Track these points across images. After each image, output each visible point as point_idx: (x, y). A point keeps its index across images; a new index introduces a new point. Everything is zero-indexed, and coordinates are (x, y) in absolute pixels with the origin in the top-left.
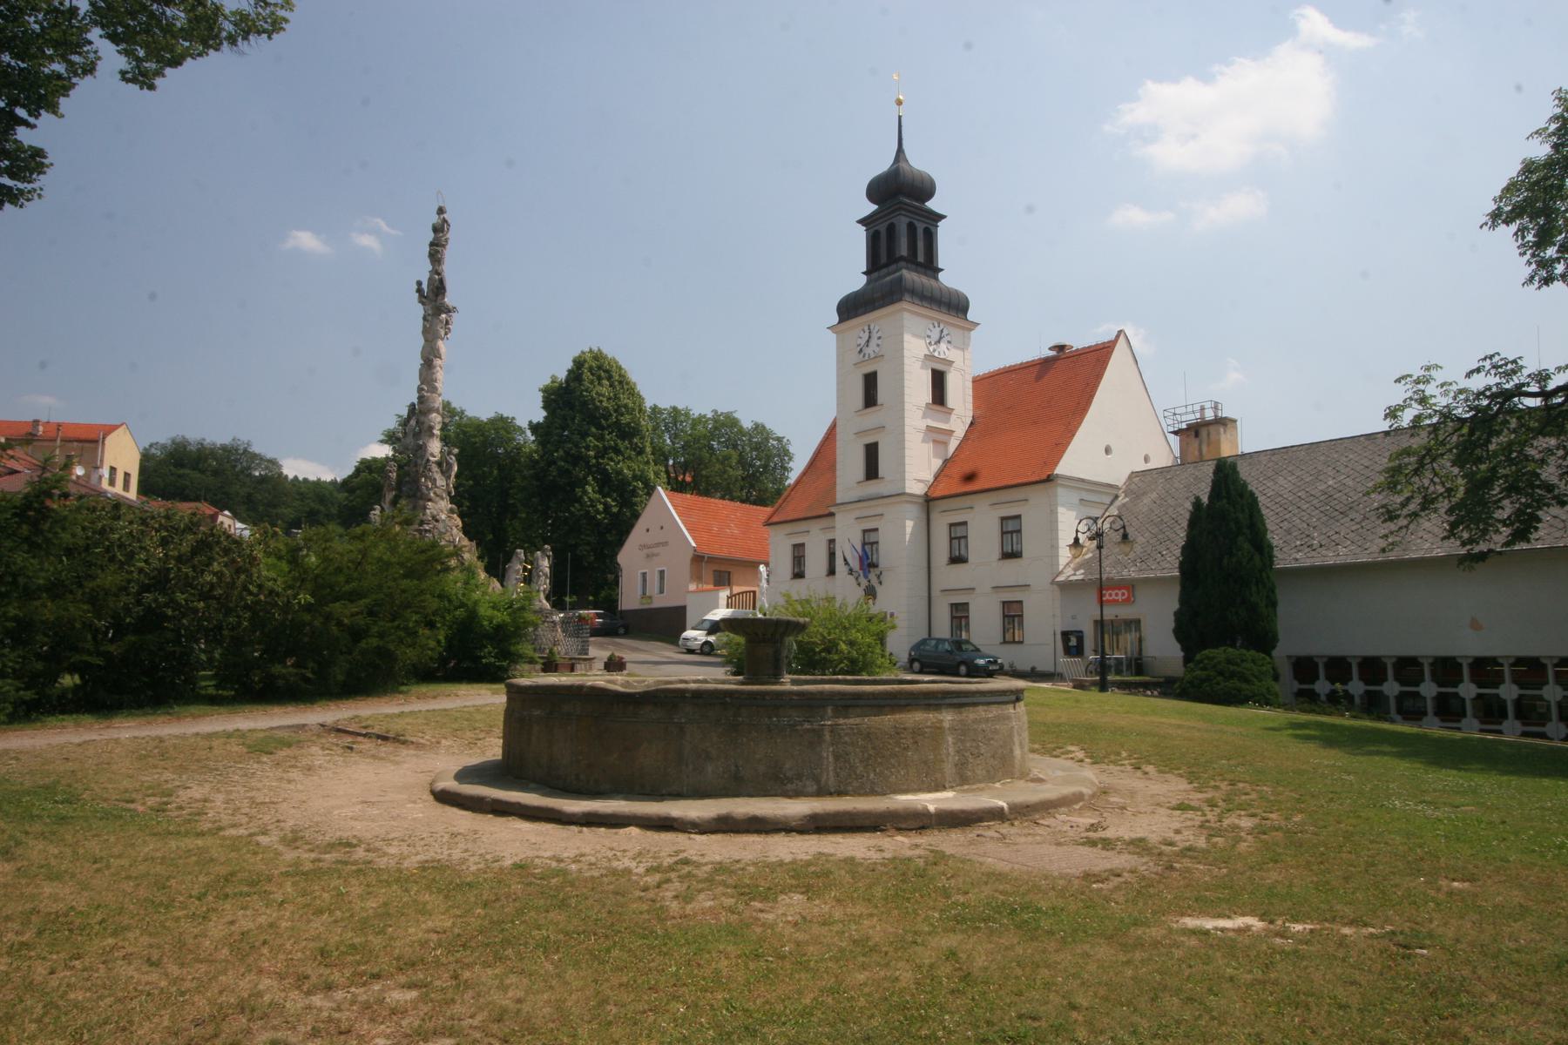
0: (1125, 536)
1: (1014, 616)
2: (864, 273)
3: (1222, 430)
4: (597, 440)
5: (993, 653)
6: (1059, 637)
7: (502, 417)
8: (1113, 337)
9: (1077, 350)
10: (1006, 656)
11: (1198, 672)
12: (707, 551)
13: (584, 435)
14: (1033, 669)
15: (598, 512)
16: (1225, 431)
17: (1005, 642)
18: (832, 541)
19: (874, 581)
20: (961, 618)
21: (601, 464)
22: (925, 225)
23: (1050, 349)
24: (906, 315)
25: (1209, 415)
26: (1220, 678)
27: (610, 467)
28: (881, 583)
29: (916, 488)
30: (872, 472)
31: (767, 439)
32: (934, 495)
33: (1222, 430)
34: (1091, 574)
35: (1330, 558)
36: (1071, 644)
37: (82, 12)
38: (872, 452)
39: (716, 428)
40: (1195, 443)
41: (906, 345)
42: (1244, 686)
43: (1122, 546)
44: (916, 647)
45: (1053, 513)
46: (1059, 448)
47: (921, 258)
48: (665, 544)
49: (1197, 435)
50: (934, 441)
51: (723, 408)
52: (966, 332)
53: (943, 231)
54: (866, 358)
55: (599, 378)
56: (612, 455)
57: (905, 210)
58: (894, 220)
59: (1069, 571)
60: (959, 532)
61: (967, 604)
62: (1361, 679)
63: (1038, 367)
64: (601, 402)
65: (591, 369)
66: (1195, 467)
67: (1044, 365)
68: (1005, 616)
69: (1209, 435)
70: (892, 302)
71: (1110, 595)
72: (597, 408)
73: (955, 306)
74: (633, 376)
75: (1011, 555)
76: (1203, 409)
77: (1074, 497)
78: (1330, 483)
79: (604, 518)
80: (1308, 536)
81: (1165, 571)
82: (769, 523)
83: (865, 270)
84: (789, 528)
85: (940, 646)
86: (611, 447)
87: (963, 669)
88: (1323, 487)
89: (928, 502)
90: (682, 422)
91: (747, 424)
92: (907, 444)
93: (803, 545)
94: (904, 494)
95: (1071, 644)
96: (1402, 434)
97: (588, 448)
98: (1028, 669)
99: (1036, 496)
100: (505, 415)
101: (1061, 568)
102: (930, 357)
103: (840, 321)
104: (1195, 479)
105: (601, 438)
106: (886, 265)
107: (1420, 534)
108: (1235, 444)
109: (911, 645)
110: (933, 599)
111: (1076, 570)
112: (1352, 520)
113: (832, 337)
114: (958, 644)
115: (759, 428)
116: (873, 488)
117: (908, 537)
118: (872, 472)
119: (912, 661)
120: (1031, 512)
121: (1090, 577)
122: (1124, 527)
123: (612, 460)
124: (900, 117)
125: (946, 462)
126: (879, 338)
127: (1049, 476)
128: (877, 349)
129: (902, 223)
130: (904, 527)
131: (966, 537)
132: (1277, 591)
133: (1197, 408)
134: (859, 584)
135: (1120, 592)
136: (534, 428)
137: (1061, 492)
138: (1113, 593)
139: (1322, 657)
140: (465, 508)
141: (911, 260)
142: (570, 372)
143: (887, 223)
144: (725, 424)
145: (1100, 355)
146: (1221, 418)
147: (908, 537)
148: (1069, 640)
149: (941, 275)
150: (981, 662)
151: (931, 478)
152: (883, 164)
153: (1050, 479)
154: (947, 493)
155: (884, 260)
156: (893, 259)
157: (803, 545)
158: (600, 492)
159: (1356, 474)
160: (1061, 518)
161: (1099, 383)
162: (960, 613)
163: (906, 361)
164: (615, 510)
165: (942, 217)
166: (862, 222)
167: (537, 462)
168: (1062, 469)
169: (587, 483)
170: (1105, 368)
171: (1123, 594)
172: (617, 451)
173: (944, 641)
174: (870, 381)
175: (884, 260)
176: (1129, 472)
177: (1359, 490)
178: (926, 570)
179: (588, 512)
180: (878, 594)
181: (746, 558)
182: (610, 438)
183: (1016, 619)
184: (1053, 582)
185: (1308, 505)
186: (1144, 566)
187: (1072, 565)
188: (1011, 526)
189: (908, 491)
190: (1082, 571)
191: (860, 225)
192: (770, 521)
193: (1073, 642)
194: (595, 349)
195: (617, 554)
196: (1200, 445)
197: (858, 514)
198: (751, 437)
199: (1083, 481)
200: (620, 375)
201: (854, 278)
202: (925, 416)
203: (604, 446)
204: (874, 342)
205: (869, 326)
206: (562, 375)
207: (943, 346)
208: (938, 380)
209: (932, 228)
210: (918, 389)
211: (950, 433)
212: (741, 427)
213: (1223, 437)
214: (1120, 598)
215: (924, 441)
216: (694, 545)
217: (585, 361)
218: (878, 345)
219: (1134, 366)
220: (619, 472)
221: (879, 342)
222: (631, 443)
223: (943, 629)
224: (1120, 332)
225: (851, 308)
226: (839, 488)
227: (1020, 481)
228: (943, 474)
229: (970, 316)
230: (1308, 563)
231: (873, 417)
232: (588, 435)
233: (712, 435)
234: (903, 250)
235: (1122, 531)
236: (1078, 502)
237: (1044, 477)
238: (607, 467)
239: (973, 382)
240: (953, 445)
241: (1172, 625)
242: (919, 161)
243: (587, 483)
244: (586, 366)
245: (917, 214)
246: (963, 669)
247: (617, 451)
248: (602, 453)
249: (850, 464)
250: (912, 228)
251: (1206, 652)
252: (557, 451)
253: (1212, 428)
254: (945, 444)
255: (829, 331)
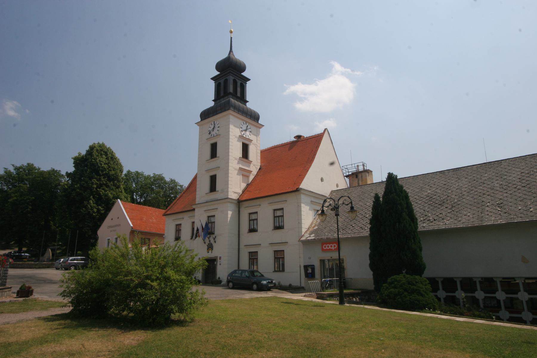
0: (352, 208)
1: (280, 258)
2: (213, 101)
3: (367, 175)
4: (97, 181)
5: (270, 277)
6: (302, 268)
7: (54, 170)
8: (322, 132)
9: (307, 137)
10: (277, 278)
11: (392, 290)
12: (138, 229)
13: (91, 178)
14: (290, 285)
15: (94, 212)
16: (368, 175)
17: (275, 271)
18: (193, 223)
19: (212, 241)
20: (254, 259)
21: (99, 191)
22: (241, 82)
23: (295, 137)
24: (231, 117)
25: (361, 169)
26: (406, 293)
27: (102, 192)
28: (215, 242)
29: (235, 196)
30: (213, 188)
31: (176, 186)
32: (242, 199)
33: (367, 175)
34: (318, 236)
35: (441, 225)
36: (308, 272)
37: (277, 284)
38: (213, 179)
39: (154, 180)
40: (356, 181)
41: (231, 130)
42: (421, 298)
43: (350, 214)
44: (231, 275)
45: (299, 207)
46: (301, 176)
47: (239, 94)
48: (119, 225)
49: (357, 177)
50: (243, 175)
51: (158, 173)
52: (258, 129)
53: (249, 85)
54: (212, 136)
55: (101, 155)
56: (105, 187)
57: (232, 73)
58: (227, 78)
59: (307, 235)
60: (253, 217)
61: (257, 252)
62: (443, 289)
63: (289, 145)
64: (101, 164)
65: (97, 150)
66: (361, 188)
67: (291, 145)
68: (275, 258)
69: (362, 177)
70: (225, 110)
71: (328, 247)
72: (99, 167)
73: (254, 117)
74: (118, 155)
75: (278, 227)
76: (358, 166)
77: (308, 199)
78: (429, 192)
79: (97, 215)
80: (426, 216)
81: (356, 234)
82: (165, 215)
83: (213, 99)
84: (174, 217)
85: (243, 274)
86: (104, 184)
87: (255, 286)
88: (426, 194)
89: (239, 202)
90: (141, 178)
91: (168, 179)
92: (230, 175)
93: (180, 225)
94: (228, 198)
95: (308, 272)
96: (459, 170)
97: (93, 183)
98: (287, 284)
99: (291, 198)
100: (55, 169)
101: (303, 233)
102: (241, 137)
103: (202, 120)
104: (362, 193)
105: (99, 180)
106: (223, 97)
107: (487, 213)
108: (372, 180)
109: (229, 273)
110: (240, 250)
111: (310, 234)
112: (446, 208)
113: (197, 128)
114: (252, 273)
115: (173, 181)
116: (214, 196)
117: (229, 219)
118: (213, 188)
119: (228, 282)
120: (288, 206)
121: (317, 238)
122: (351, 203)
123: (103, 189)
124: (231, 38)
125: (248, 185)
126: (219, 127)
127: (297, 188)
128: (217, 132)
129: (231, 79)
130: (227, 214)
131: (257, 219)
132: (421, 242)
133: (356, 165)
134: (205, 243)
135: (333, 245)
136: (68, 175)
137: (303, 196)
138: (330, 246)
139: (440, 278)
140: (29, 210)
141: (234, 95)
142: (87, 151)
143: (224, 79)
144: (159, 180)
145: (317, 139)
146: (366, 170)
147: (229, 219)
148: (308, 270)
149: (247, 104)
150: (264, 282)
151: (240, 192)
152: (224, 55)
153: (298, 190)
154: (248, 198)
155: (222, 94)
156: (227, 94)
157: (180, 225)
158: (96, 203)
159: (441, 188)
160: (303, 209)
161: (318, 149)
162: (253, 257)
163: (231, 137)
164: (103, 212)
165: (249, 80)
166: (212, 79)
167: (67, 189)
168: (303, 186)
169: (90, 199)
170: (320, 143)
171: (335, 246)
172: (107, 186)
173: (245, 271)
174: (214, 147)
175: (222, 94)
176: (331, 191)
177: (445, 194)
178: (237, 236)
179: (90, 212)
180: (214, 248)
181: (158, 232)
182: (104, 180)
183: (255, 260)
184: (299, 241)
185: (421, 202)
186: (345, 232)
187: (308, 232)
188: (279, 213)
189: (229, 197)
190: (313, 235)
191: (212, 81)
192: (166, 213)
193: (310, 271)
194: (101, 143)
195: (97, 231)
196: (358, 181)
197: (206, 208)
198: (169, 185)
199: (312, 192)
200: (112, 155)
201: (209, 103)
202: (238, 163)
203: (100, 183)
204: (215, 130)
205: (214, 122)
206: (84, 153)
207: (248, 133)
208: (245, 148)
209: (244, 84)
210: (236, 150)
211: (250, 172)
212: (165, 180)
213: (368, 178)
214: (333, 248)
215: (238, 174)
216: (132, 225)
217: (95, 147)
218: (218, 130)
219: (331, 145)
220: (106, 195)
221: (219, 129)
222: (114, 183)
223: (245, 265)
224: (326, 129)
225: (206, 115)
226: (197, 196)
227: (283, 192)
228: (246, 190)
229: (260, 122)
230: (431, 228)
231: (215, 163)
232: (93, 178)
233: (153, 184)
234: (231, 89)
235: (350, 205)
236: (309, 202)
237: (295, 189)
238: (101, 193)
239: (261, 152)
240: (251, 178)
241: (368, 262)
242: (239, 56)
243: (90, 199)
244: (95, 149)
245: (238, 76)
246: (255, 286)
247: (107, 186)
248: (100, 186)
249: (204, 185)
250: (235, 82)
251: (394, 277)
252: (76, 185)
253: (363, 174)
254: (248, 177)
255: (196, 125)
